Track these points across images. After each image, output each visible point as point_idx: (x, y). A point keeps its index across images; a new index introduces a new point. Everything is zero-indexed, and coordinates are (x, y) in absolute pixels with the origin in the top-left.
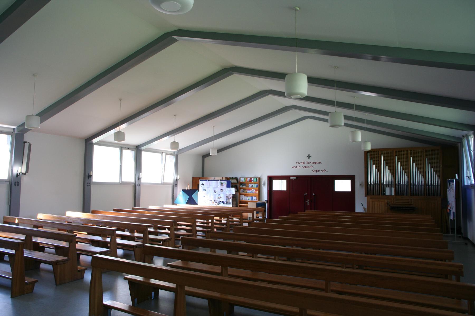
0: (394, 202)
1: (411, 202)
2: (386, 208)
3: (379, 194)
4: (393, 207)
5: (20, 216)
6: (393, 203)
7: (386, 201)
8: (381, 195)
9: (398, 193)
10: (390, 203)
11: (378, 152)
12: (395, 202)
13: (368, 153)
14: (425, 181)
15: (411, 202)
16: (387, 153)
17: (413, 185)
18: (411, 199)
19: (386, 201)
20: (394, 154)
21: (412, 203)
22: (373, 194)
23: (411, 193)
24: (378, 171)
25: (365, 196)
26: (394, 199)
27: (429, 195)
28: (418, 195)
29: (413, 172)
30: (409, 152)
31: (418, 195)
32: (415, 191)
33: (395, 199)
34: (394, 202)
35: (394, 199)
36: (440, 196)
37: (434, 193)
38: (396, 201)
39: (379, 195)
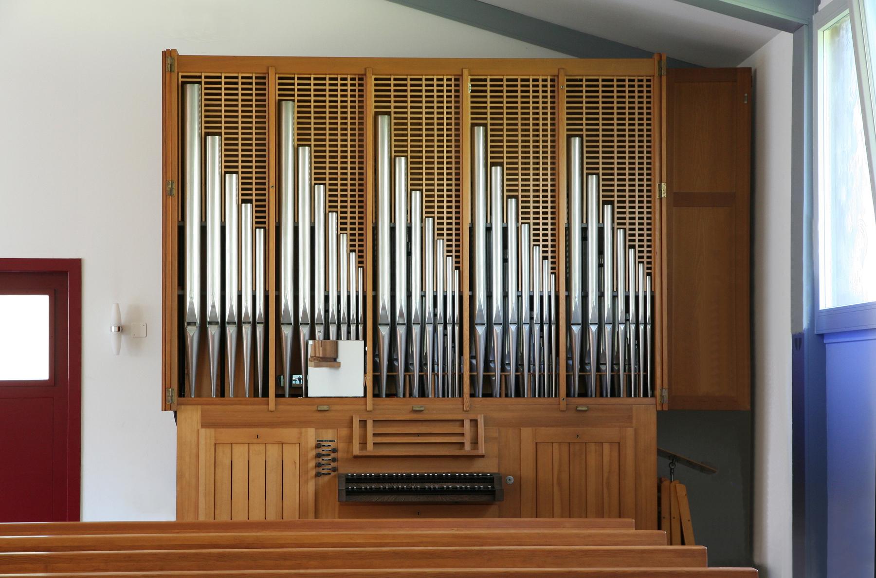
0: (363, 444)
1: (475, 442)
2: (311, 487)
3: (260, 391)
4: (359, 479)
5: (277, 398)
6: (356, 451)
7: (311, 436)
8: (280, 395)
9: (392, 379)
10: (334, 451)
11: (262, 81)
12: (370, 440)
13: (189, 87)
14: (563, 294)
15: (475, 442)
16: (320, 93)
17: (198, 319)
18: (475, 422)
19: (311, 436)
20: (467, 119)
21: (482, 450)
22: (222, 392)
23: (473, 379)
24: (260, 222)
25: (165, 408)
26: (363, 423)
27: (583, 394)
28: (519, 393)
29: (393, 230)
30: (468, 87)
31: (519, 393)
32: (497, 365)
33: (370, 424)
34: (363, 444)
35: (363, 423)
36: (653, 396)
37: (615, 378)
38: (374, 435)
39: (266, 394)
